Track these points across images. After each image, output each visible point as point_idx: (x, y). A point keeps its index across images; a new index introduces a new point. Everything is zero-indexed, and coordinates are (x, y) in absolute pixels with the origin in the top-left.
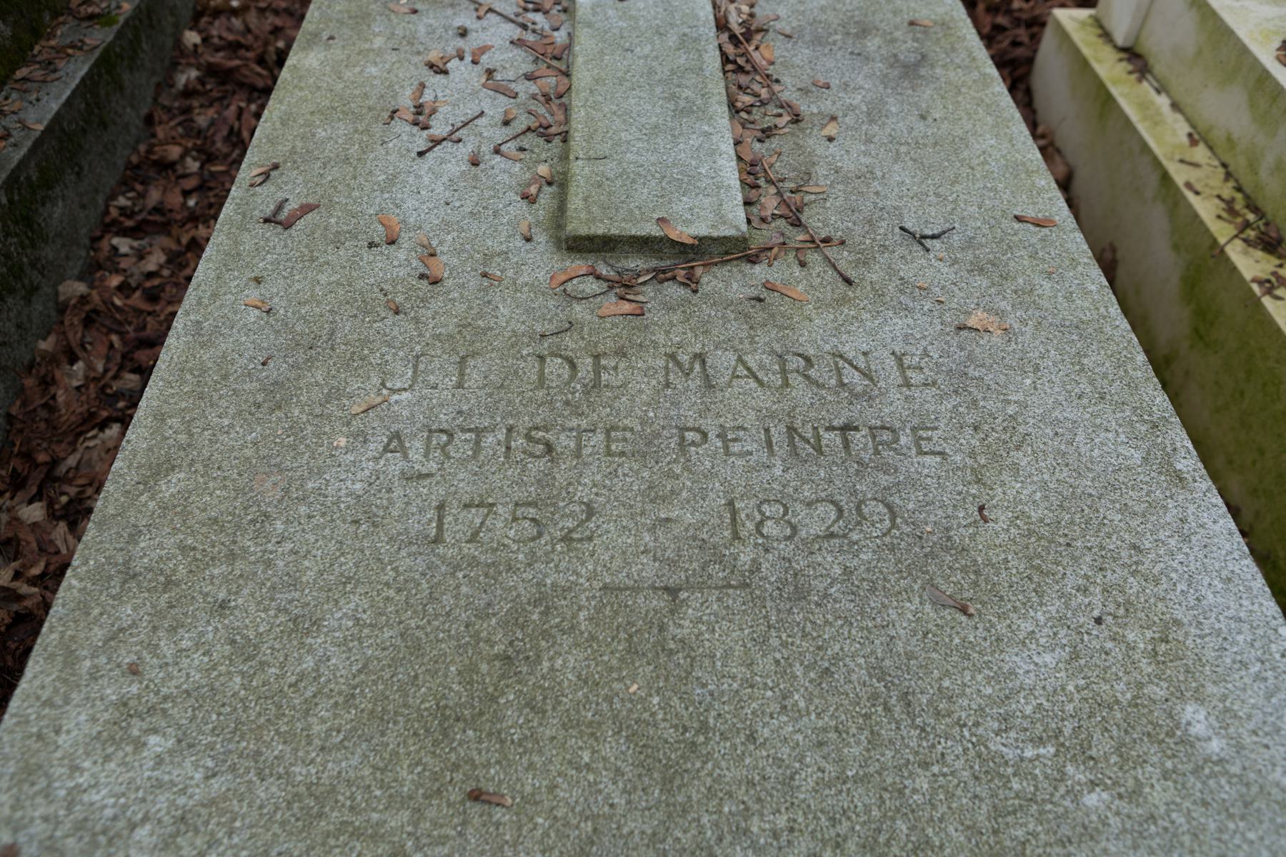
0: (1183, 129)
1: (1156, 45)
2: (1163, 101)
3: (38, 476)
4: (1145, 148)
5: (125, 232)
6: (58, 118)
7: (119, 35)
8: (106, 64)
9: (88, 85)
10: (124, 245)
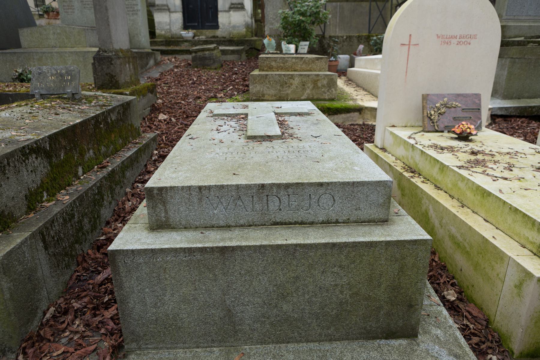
0: (394, 158)
1: (387, 146)
2: (390, 155)
3: (121, 219)
4: (386, 162)
5: (139, 183)
6: (131, 155)
7: (143, 146)
8: (139, 150)
9: (136, 152)
10: (140, 185)
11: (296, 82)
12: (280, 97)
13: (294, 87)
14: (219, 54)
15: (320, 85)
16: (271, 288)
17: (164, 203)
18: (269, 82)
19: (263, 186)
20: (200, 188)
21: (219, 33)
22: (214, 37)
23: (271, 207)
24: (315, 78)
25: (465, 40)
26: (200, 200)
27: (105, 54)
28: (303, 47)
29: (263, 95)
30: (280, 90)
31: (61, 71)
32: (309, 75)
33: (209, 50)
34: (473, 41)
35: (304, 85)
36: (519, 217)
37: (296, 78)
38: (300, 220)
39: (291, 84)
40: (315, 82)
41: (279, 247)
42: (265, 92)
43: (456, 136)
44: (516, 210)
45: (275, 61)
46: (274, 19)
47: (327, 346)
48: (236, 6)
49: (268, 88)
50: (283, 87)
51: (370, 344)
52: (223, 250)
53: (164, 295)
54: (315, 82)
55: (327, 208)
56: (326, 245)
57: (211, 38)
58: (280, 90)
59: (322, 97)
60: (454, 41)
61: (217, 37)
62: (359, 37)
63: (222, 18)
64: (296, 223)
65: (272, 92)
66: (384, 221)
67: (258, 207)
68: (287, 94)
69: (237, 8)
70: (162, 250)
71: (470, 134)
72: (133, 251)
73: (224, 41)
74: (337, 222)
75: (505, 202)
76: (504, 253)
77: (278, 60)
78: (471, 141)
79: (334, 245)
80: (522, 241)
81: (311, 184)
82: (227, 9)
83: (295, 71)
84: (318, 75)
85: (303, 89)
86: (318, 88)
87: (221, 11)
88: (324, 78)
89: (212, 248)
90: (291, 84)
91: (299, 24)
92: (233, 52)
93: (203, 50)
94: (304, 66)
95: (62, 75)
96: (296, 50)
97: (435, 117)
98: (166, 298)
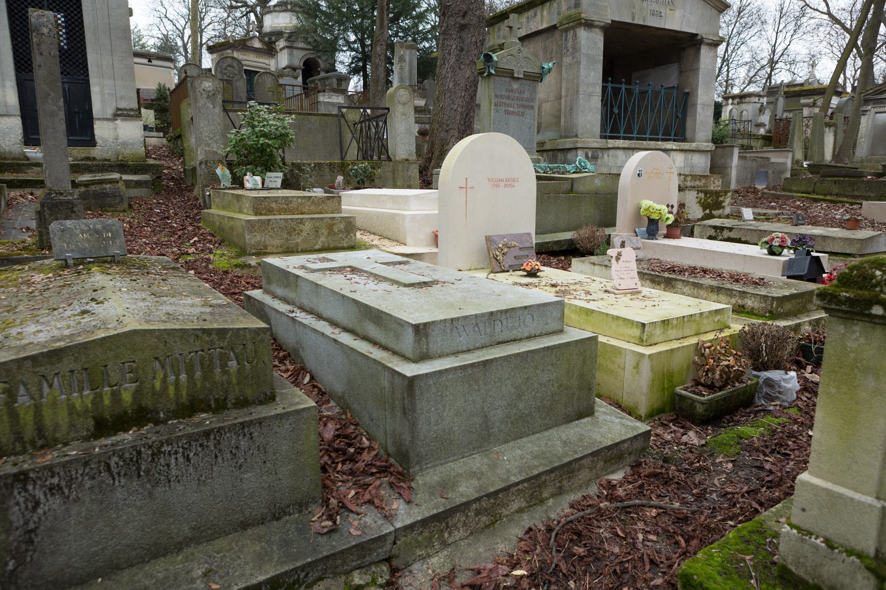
11: (307, 227)
12: (288, 248)
13: (304, 234)
14: (123, 188)
15: (336, 230)
16: (513, 390)
17: (427, 336)
18: (273, 229)
19: (492, 313)
20: (452, 320)
21: (96, 152)
22: (88, 159)
23: (497, 330)
24: (330, 222)
25: (510, 183)
26: (451, 330)
27: (61, 198)
28: (272, 179)
29: (266, 247)
30: (287, 240)
31: (95, 226)
32: (322, 219)
33: (111, 181)
34: (516, 184)
35: (317, 231)
36: (620, 322)
37: (307, 223)
38: (513, 338)
39: (301, 231)
40: (330, 227)
41: (518, 354)
42: (268, 243)
43: (525, 273)
44: (618, 317)
45: (276, 202)
46: (211, 139)
47: (546, 434)
48: (125, 112)
49: (272, 237)
50: (291, 236)
51: (570, 425)
52: (485, 363)
53: (444, 411)
54: (330, 227)
55: (532, 326)
56: (544, 348)
57: (82, 160)
58: (287, 240)
59: (340, 245)
60: (502, 184)
61: (94, 159)
62: (331, 164)
63: (101, 130)
64: (512, 341)
65: (277, 242)
66: (561, 331)
67: (488, 330)
68: (297, 244)
69: (129, 116)
70: (446, 370)
71: (539, 270)
72: (427, 374)
73: (110, 166)
74: (535, 336)
75: (607, 314)
76: (621, 348)
77: (280, 201)
78: (538, 277)
79: (548, 347)
80: (627, 339)
81: (520, 308)
82: (109, 117)
83: (302, 214)
84: (333, 218)
85: (317, 236)
86: (335, 234)
87: (99, 119)
88: (341, 222)
89: (478, 362)
90: (301, 231)
91: (262, 150)
92: (138, 184)
93: (101, 182)
94: (313, 207)
95: (97, 232)
96: (263, 184)
97: (500, 257)
98: (445, 414)
